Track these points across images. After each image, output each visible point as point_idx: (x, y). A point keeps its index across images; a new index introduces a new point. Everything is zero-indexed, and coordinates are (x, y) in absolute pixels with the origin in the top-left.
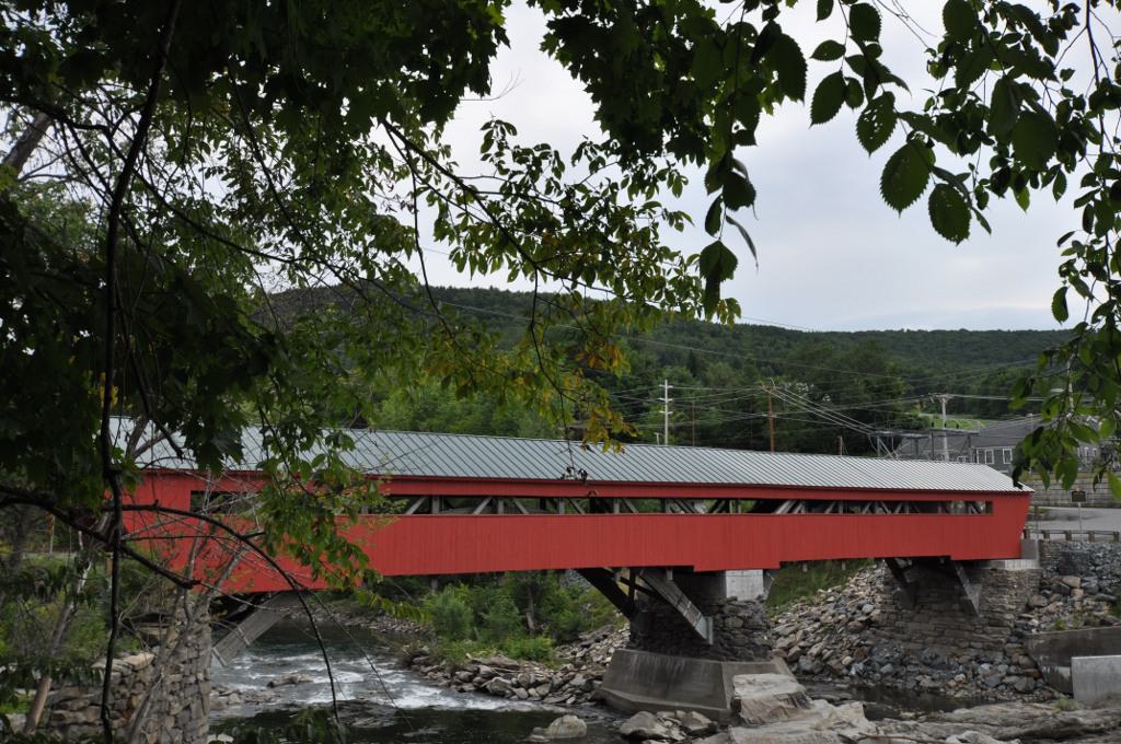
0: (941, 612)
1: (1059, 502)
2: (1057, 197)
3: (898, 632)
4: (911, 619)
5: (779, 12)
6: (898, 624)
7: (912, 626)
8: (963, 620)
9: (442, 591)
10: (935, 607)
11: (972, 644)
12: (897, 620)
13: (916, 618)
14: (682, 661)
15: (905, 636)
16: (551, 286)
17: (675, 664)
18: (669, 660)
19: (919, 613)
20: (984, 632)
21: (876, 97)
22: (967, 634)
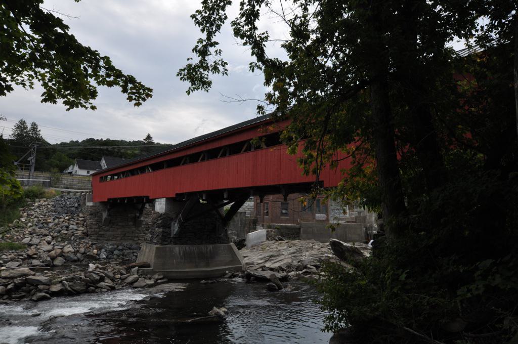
0: (123, 226)
1: (82, 187)
2: (42, 102)
3: (101, 237)
4: (108, 230)
5: (89, 47)
6: (100, 233)
7: (108, 233)
8: (134, 229)
9: (307, 151)
10: (120, 224)
11: (140, 238)
12: (99, 231)
13: (111, 230)
14: (210, 247)
15: (106, 238)
16: (342, 242)
17: (207, 248)
18: (203, 247)
19: (111, 227)
20: (144, 233)
21: (496, 326)
22: (137, 235)
